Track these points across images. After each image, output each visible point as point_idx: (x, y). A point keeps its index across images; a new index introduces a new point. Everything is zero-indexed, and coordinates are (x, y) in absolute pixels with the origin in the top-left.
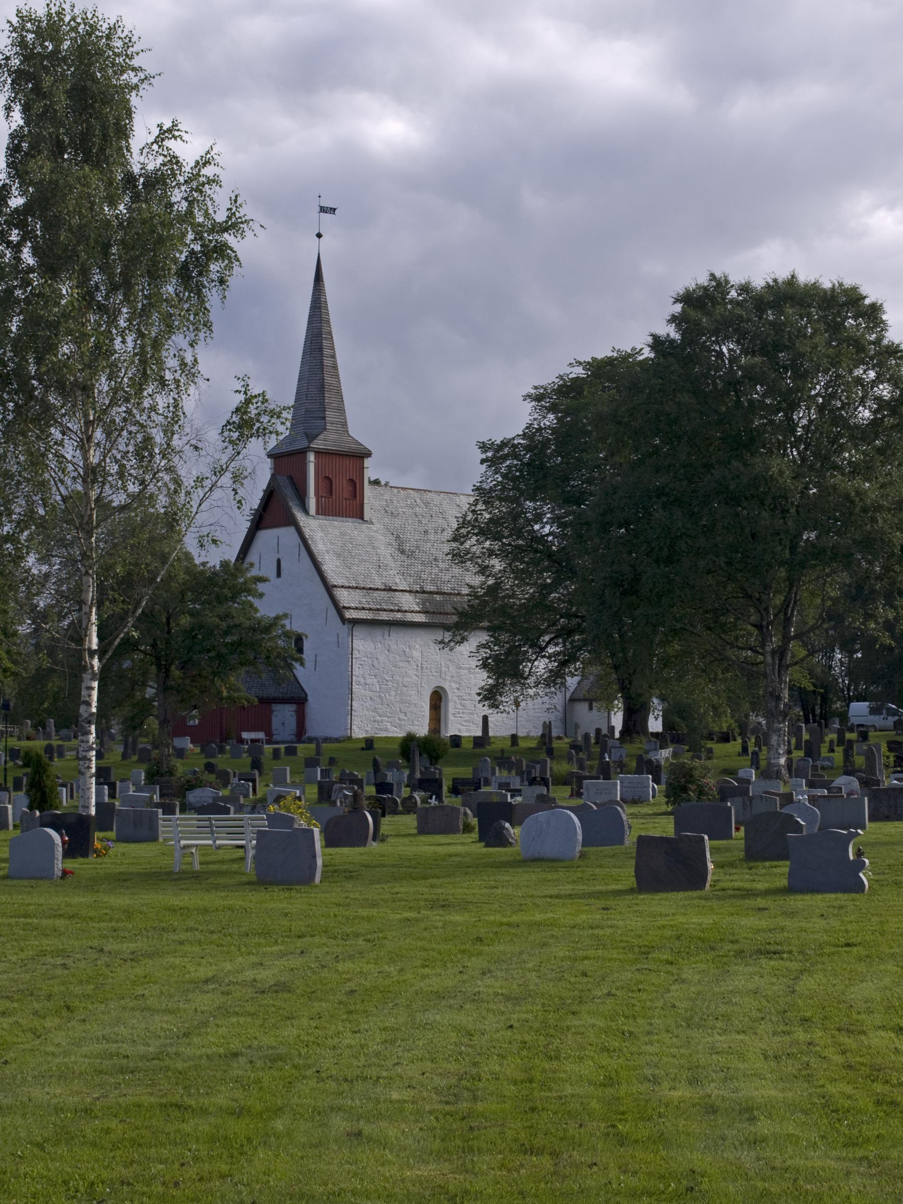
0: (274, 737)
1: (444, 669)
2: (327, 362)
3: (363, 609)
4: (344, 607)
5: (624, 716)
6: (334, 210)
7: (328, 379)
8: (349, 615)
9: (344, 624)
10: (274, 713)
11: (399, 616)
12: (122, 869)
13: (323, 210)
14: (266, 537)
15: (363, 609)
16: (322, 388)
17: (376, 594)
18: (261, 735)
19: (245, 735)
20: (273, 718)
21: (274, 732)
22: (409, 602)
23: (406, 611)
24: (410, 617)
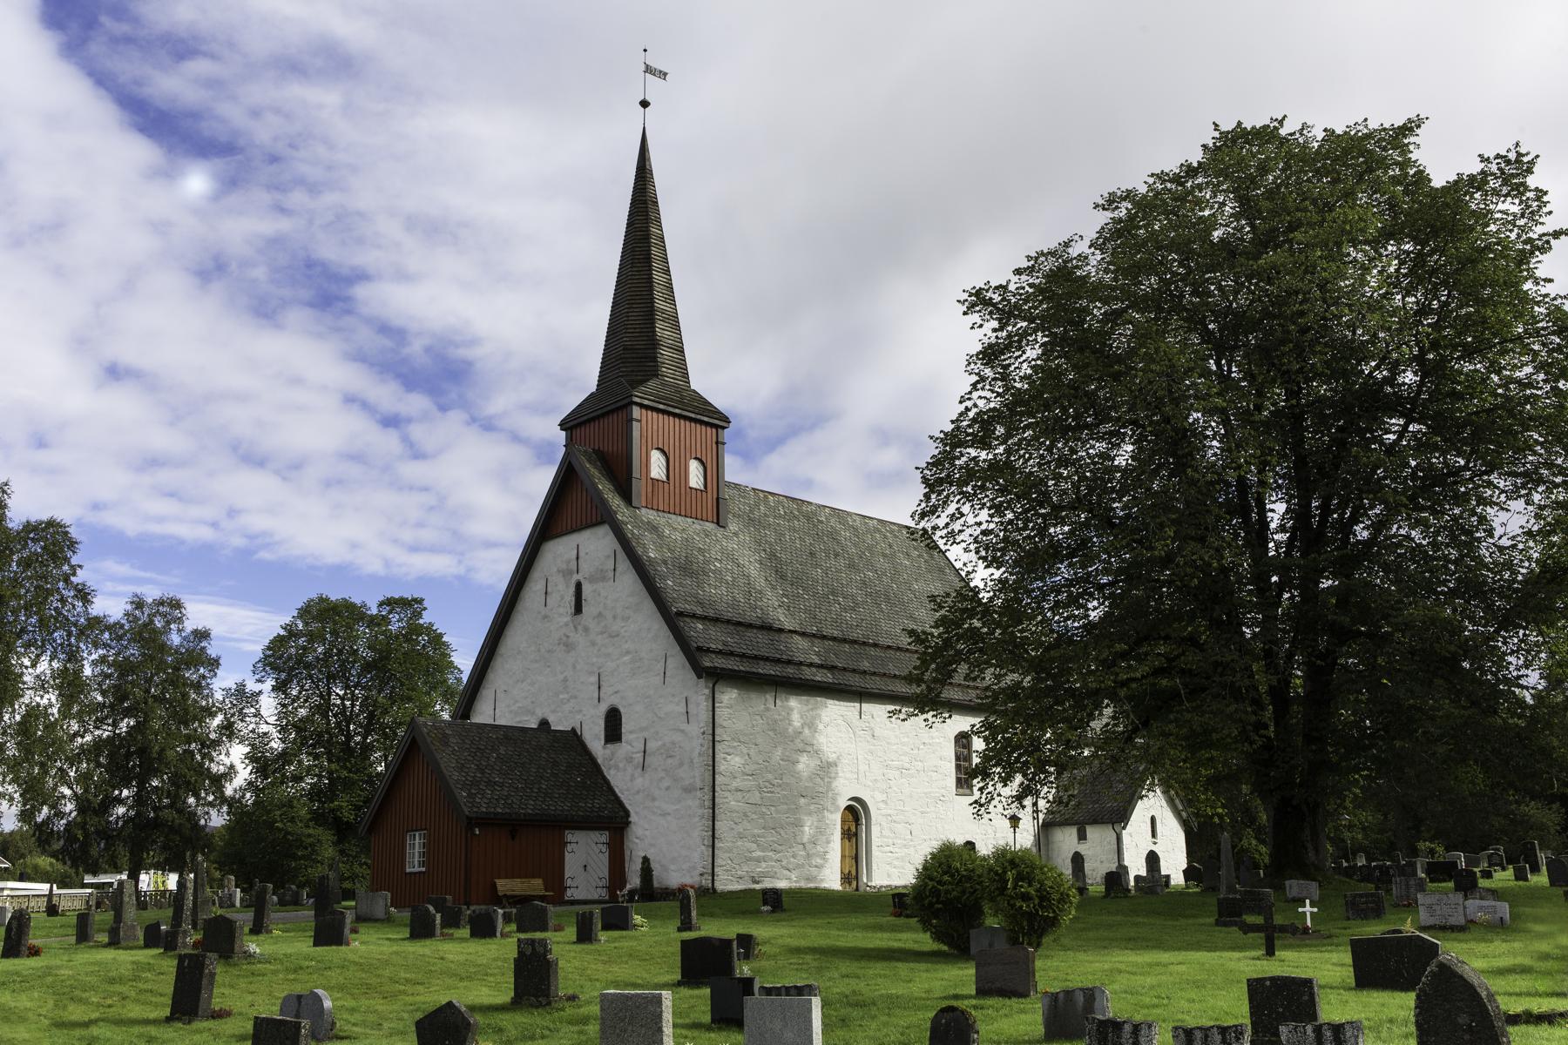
0: (569, 892)
1: (863, 768)
2: (658, 277)
3: (732, 654)
4: (699, 649)
5: (1171, 802)
6: (665, 74)
7: (660, 304)
8: (707, 662)
9: (699, 677)
10: (569, 847)
11: (790, 670)
12: (1008, 1002)
13: (649, 70)
14: (559, 551)
15: (732, 654)
16: (650, 314)
17: (750, 634)
18: (535, 886)
19: (504, 885)
20: (568, 856)
21: (569, 883)
22: (802, 648)
23: (801, 663)
24: (808, 673)
